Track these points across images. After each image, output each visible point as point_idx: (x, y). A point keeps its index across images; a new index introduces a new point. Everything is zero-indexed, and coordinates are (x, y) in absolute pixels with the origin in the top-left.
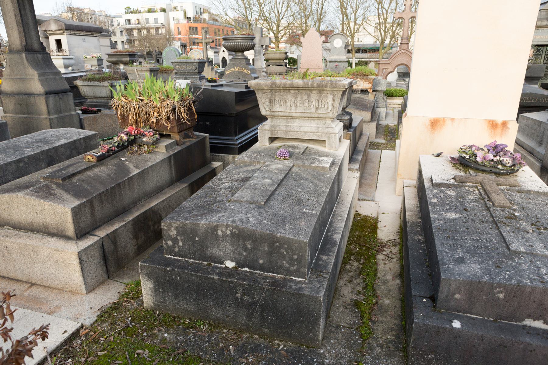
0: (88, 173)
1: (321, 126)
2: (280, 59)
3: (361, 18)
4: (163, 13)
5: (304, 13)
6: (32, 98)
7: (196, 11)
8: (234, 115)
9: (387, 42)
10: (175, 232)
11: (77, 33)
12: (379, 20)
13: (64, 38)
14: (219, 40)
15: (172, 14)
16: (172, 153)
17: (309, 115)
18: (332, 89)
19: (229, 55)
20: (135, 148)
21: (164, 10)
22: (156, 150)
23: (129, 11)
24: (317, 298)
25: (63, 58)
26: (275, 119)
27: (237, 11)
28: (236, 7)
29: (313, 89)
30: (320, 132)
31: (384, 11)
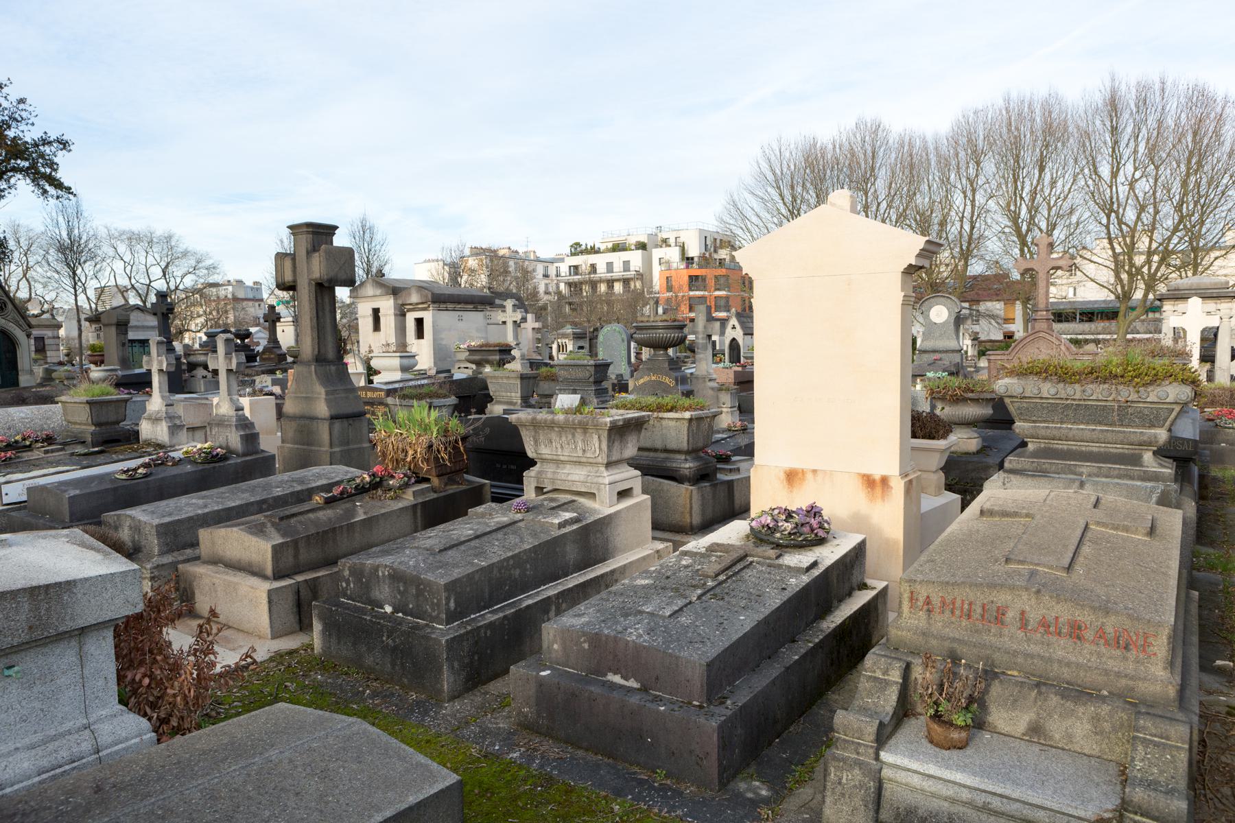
0: (311, 516)
4: (640, 251)
6: (315, 423)
7: (706, 245)
9: (1138, 295)
10: (348, 572)
11: (450, 306)
13: (428, 316)
15: (657, 253)
16: (420, 500)
20: (380, 492)
21: (642, 246)
22: (404, 496)
23: (577, 249)
24: (440, 641)
25: (401, 357)
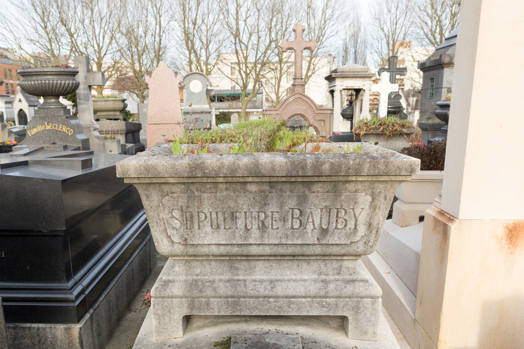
1: (331, 277)
2: (114, 110)
3: (214, 55)
5: (136, 47)
8: (62, 234)
9: (250, 87)
12: (238, 57)
14: (12, 84)
17: (297, 250)
18: (374, 179)
19: (30, 106)
26: (198, 263)
27: (37, 44)
28: (36, 37)
29: (316, 179)
30: (331, 294)
31: (243, 46)
